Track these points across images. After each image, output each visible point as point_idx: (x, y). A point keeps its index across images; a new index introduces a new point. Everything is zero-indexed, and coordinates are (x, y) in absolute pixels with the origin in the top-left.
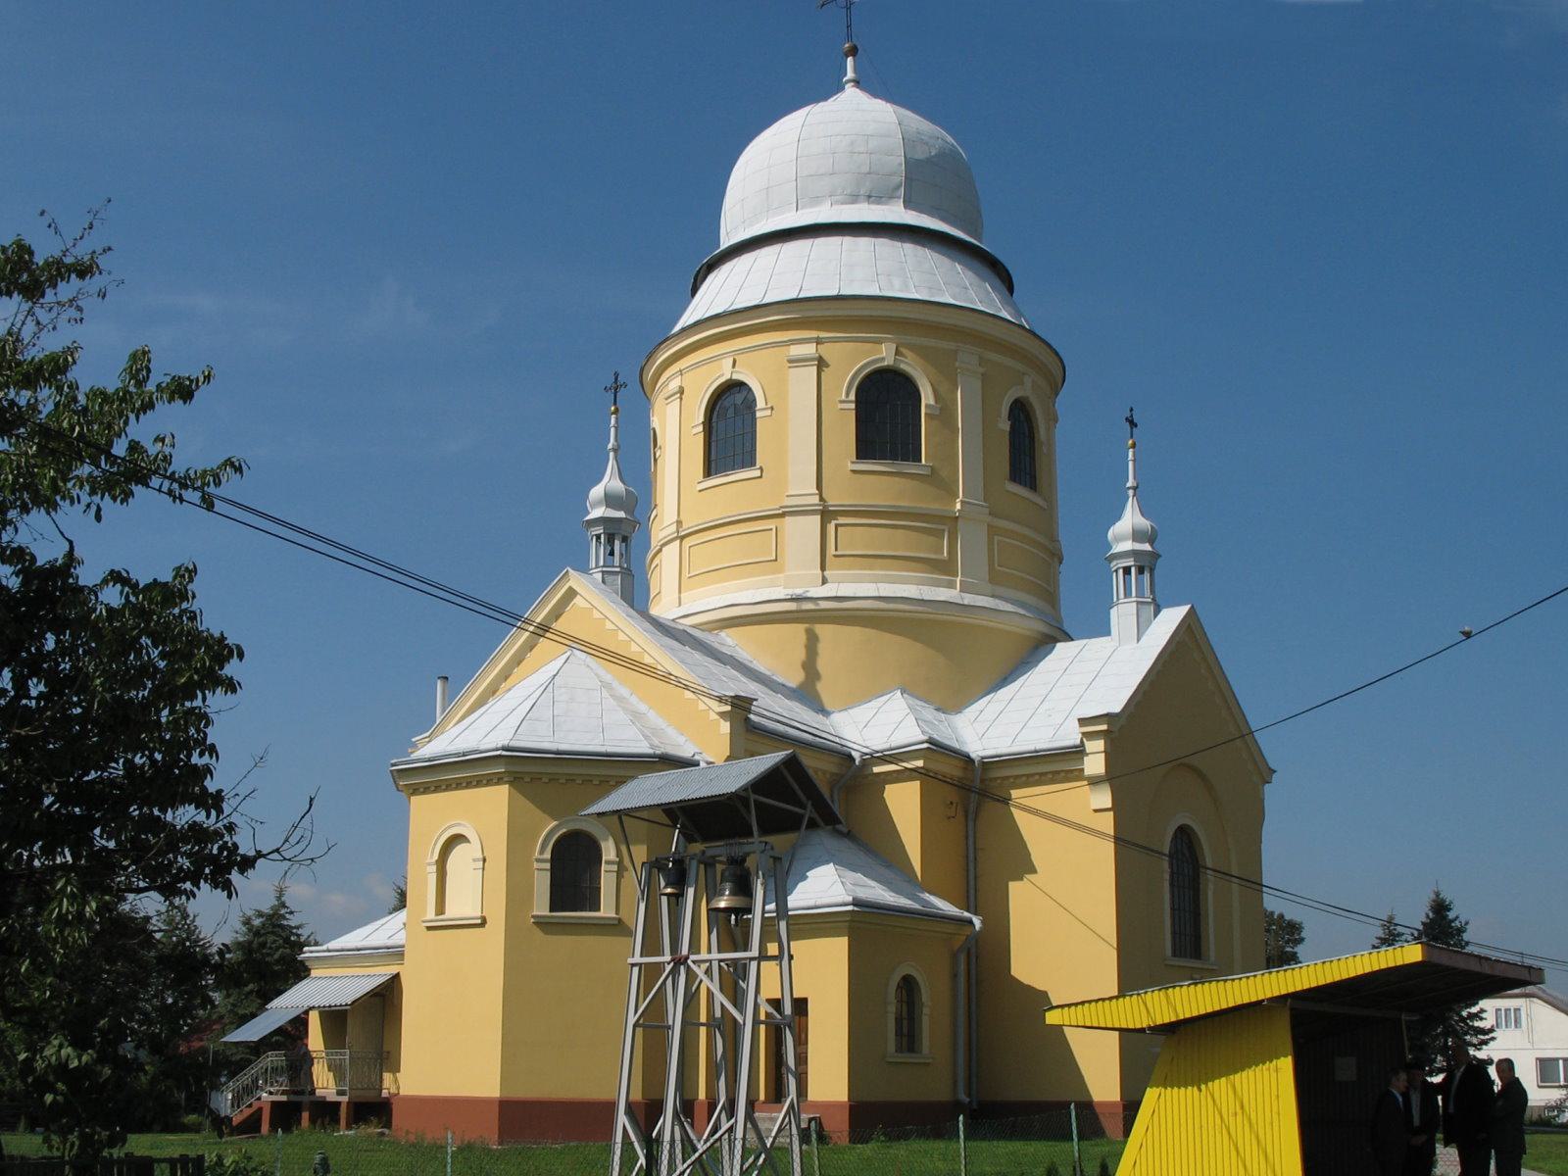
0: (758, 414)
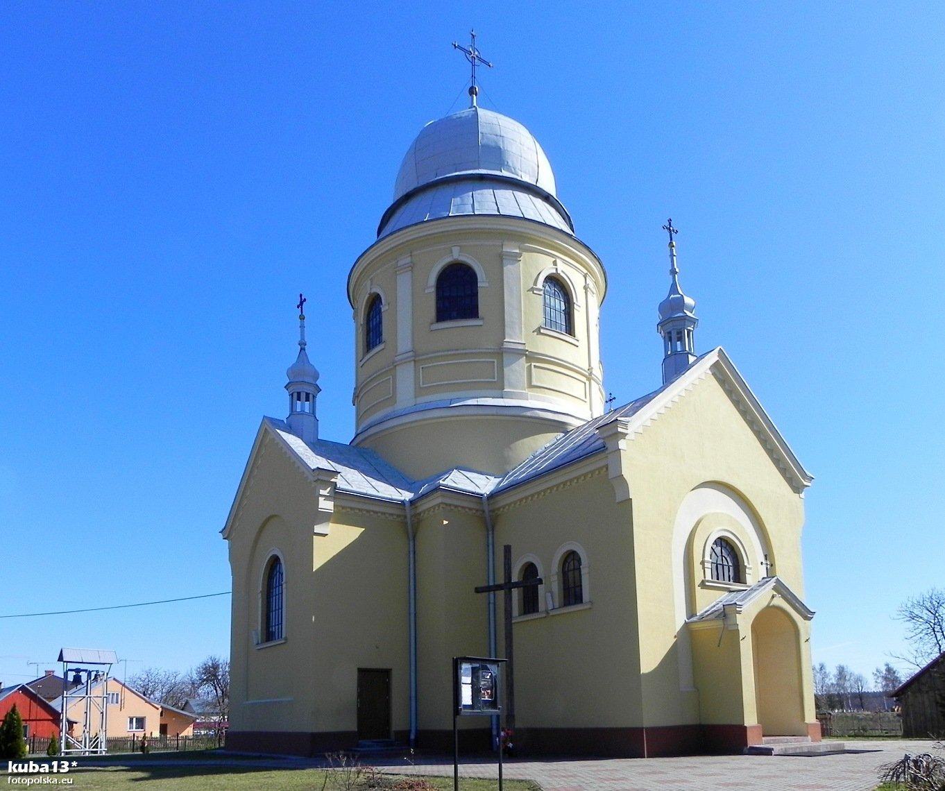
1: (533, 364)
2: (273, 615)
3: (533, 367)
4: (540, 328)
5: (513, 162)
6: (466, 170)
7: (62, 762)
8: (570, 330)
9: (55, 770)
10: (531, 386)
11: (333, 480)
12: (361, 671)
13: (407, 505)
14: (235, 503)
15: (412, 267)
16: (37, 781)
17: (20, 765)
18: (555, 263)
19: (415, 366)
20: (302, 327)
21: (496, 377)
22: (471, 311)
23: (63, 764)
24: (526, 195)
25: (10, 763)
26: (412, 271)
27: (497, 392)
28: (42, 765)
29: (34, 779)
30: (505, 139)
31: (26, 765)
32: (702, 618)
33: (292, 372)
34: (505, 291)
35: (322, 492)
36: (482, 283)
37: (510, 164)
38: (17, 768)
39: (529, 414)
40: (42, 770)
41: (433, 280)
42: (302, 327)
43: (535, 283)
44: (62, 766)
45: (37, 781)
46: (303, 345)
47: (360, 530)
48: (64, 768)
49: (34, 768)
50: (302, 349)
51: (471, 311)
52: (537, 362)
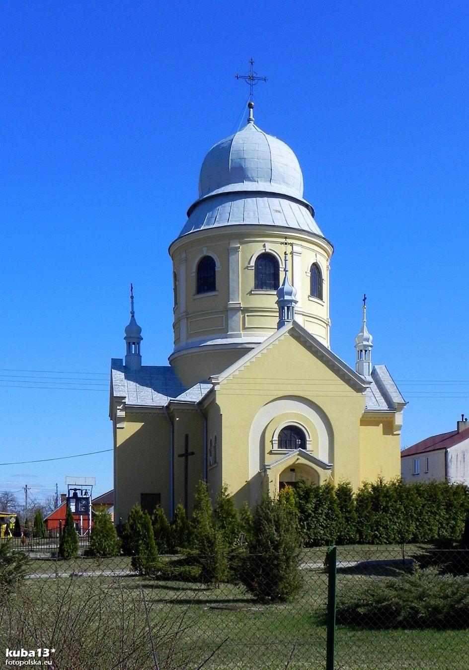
1: (246, 314)
3: (246, 316)
4: (251, 291)
5: (251, 174)
7: (44, 649)
9: (39, 655)
10: (245, 328)
11: (123, 401)
12: (142, 494)
13: (164, 409)
16: (26, 663)
17: (15, 652)
18: (264, 246)
20: (132, 303)
23: (45, 651)
25: (7, 650)
28: (30, 652)
29: (24, 664)
30: (246, 160)
31: (19, 652)
33: (127, 330)
34: (230, 272)
35: (118, 407)
36: (218, 269)
37: (250, 176)
38: (12, 653)
39: (239, 347)
40: (30, 655)
42: (132, 303)
43: (249, 263)
44: (45, 652)
45: (26, 663)
46: (133, 313)
47: (141, 424)
48: (46, 654)
49: (24, 653)
50: (133, 316)
52: (249, 313)
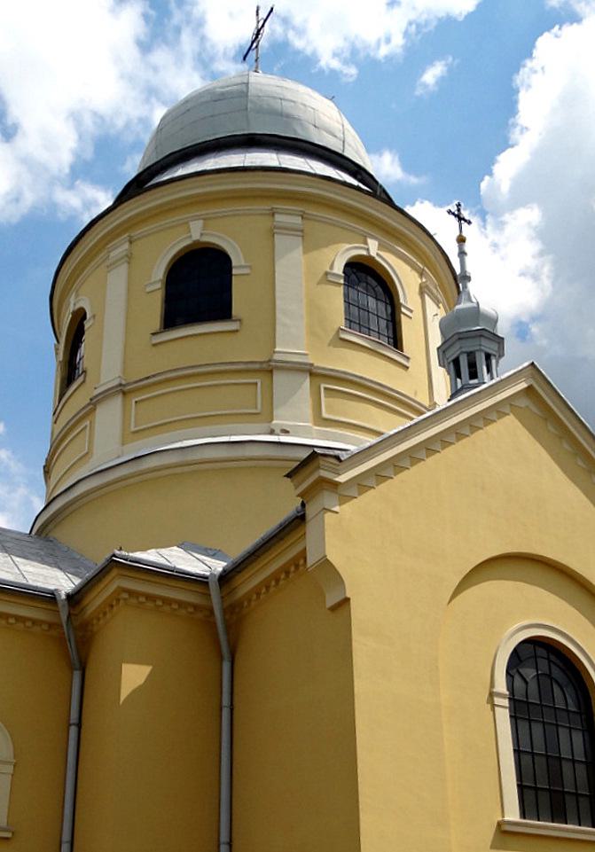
0: (234, 272)
2: (275, 539)
6: (173, 443)
8: (396, 342)
14: (46, 512)
15: (129, 258)
19: (124, 406)
21: (259, 406)
22: (219, 308)
24: (302, 160)
26: (129, 263)
27: (265, 426)
32: (579, 708)
41: (159, 273)
51: (219, 308)
